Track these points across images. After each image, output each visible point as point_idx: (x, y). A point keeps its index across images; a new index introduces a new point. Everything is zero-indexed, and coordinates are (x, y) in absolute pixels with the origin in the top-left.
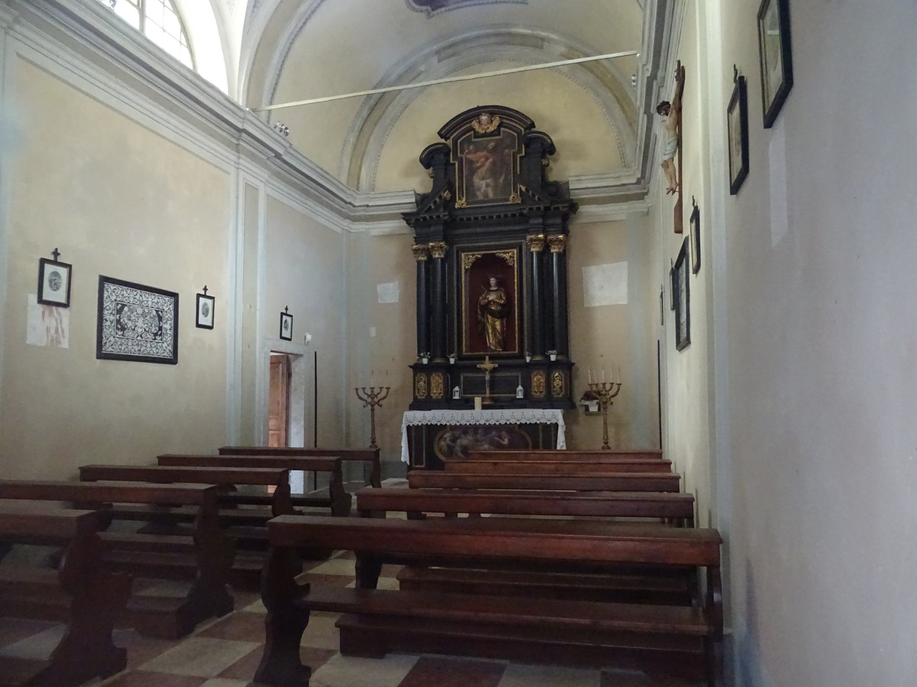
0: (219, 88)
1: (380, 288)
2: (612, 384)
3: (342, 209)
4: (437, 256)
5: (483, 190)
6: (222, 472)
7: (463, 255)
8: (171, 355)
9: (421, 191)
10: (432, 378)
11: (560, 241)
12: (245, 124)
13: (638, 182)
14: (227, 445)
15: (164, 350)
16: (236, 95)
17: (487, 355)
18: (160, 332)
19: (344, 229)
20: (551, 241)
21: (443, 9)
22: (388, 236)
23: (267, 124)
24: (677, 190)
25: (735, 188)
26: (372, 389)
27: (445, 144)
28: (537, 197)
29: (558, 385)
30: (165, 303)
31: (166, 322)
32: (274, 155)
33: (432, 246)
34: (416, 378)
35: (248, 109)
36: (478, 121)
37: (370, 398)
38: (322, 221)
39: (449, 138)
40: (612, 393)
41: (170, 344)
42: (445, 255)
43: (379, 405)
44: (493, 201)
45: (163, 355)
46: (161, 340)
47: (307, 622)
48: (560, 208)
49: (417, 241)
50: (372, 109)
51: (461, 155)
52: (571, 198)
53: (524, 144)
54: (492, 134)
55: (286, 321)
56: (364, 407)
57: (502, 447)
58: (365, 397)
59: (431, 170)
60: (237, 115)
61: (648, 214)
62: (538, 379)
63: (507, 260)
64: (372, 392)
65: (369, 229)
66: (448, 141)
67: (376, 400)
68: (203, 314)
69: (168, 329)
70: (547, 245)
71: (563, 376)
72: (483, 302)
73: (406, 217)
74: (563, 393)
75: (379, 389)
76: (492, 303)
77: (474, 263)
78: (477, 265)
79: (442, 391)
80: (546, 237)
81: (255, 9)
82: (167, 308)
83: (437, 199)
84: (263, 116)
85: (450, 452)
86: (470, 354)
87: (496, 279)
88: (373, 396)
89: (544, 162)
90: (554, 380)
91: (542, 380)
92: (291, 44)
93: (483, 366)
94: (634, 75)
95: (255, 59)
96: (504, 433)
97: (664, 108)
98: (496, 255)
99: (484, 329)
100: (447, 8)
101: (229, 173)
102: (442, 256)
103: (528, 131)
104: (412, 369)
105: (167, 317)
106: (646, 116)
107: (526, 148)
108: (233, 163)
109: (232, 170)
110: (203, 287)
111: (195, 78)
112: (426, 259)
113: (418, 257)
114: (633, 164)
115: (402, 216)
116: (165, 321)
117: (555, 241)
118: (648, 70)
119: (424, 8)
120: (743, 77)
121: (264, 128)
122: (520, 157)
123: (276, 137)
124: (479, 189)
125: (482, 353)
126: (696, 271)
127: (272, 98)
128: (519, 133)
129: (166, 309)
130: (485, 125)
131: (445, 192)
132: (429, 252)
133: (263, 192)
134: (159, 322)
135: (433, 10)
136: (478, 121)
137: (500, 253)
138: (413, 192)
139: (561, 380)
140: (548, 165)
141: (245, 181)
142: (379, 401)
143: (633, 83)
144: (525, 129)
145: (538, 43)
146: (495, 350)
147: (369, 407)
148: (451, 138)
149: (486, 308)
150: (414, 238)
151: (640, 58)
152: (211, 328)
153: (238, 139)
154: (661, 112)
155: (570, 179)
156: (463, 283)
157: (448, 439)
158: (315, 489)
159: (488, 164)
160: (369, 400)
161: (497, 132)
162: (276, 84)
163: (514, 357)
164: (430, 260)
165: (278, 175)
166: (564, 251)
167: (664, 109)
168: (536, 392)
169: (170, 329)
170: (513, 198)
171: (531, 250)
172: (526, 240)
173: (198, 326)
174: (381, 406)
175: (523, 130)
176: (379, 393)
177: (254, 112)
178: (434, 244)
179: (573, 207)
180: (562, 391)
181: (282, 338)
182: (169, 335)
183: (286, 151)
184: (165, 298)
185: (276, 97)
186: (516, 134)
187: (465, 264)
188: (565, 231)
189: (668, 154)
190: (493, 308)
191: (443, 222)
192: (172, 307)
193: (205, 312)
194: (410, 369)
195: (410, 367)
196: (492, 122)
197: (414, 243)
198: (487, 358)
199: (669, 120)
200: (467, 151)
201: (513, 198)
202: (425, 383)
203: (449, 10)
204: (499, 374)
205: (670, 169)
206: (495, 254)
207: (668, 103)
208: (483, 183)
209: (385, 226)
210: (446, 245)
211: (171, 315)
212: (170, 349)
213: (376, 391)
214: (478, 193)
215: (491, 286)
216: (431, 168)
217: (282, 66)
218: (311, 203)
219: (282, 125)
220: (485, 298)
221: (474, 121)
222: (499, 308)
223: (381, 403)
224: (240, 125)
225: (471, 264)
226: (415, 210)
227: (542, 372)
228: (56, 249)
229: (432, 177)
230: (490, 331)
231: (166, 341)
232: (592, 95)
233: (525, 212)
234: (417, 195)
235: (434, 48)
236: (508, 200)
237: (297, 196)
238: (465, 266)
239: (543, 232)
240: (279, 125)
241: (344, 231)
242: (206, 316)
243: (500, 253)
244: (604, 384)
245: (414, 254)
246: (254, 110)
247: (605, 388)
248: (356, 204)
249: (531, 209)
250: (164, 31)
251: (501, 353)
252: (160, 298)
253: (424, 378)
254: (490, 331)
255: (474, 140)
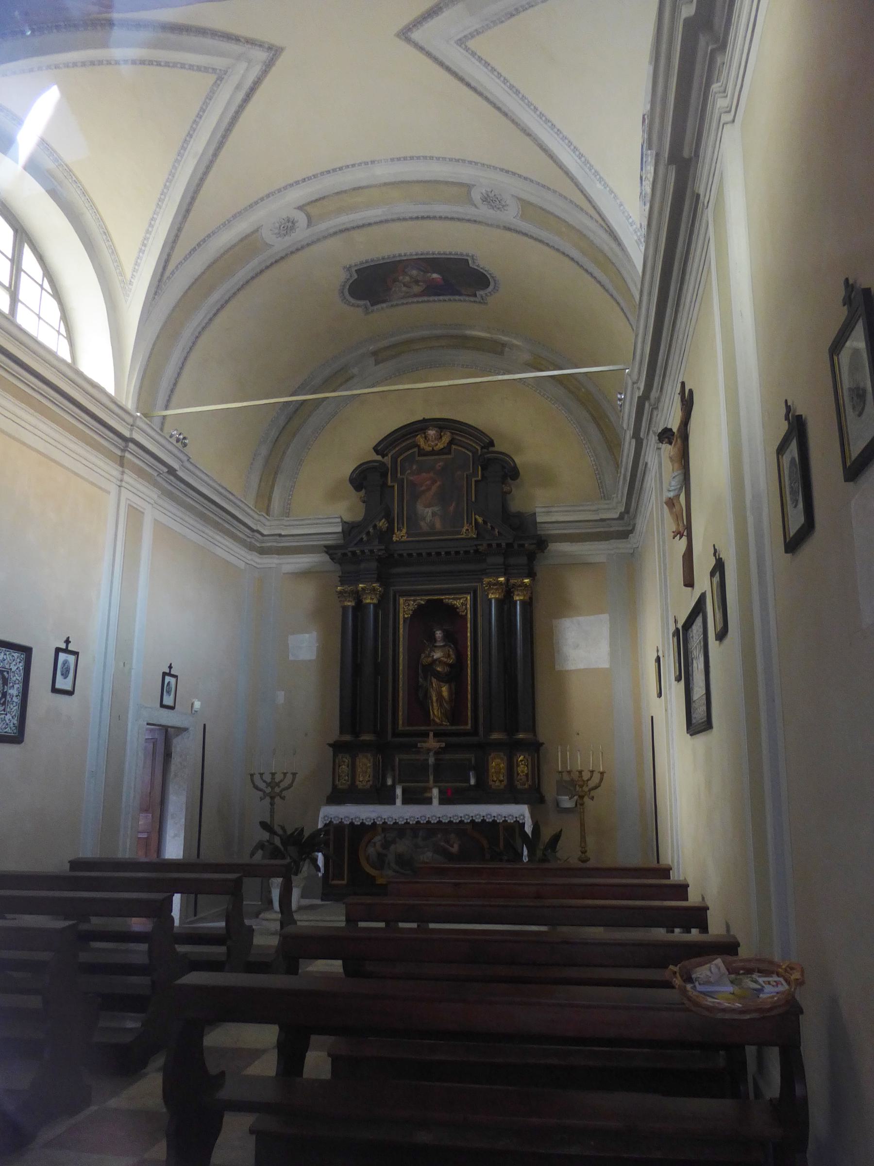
0: (99, 382)
1: (292, 640)
2: (592, 772)
3: (263, 545)
4: (368, 601)
5: (428, 519)
6: (86, 900)
7: (401, 601)
8: (15, 731)
9: (348, 518)
10: (358, 760)
11: (526, 586)
12: (134, 432)
13: (621, 517)
14: (81, 856)
15: (7, 724)
16: (125, 396)
17: (432, 731)
18: (4, 699)
19: (248, 564)
20: (514, 585)
21: (384, 305)
22: (305, 574)
23: (159, 431)
24: (685, 533)
25: (793, 545)
26: (273, 774)
27: (381, 461)
28: (497, 531)
29: (523, 772)
30: (14, 660)
31: (13, 686)
32: (166, 470)
33: (362, 588)
34: (337, 761)
35: (139, 414)
36: (423, 436)
37: (269, 787)
38: (219, 552)
39: (387, 455)
40: (592, 784)
41: (15, 715)
42: (379, 601)
43: (280, 797)
44: (441, 533)
45: (5, 731)
46: (4, 710)
47: (219, 1130)
48: (526, 545)
49: (343, 581)
50: (290, 419)
51: (401, 477)
52: (539, 533)
53: (481, 466)
54: (441, 452)
55: (169, 683)
56: (261, 799)
57: (450, 857)
58: (262, 785)
59: (362, 493)
60: (124, 421)
61: (632, 554)
62: (497, 764)
63: (457, 608)
64: (273, 778)
65: (280, 564)
66: (386, 458)
67: (277, 790)
68: (62, 675)
69: (15, 695)
70: (509, 592)
71: (530, 760)
72: (425, 661)
73: (329, 550)
74: (530, 782)
75: (282, 775)
76: (437, 662)
77: (415, 612)
78: (420, 612)
79: (371, 778)
80: (507, 580)
81: (156, 297)
82: (16, 667)
83: (371, 530)
84: (157, 422)
85: (380, 862)
86: (408, 728)
87: (443, 632)
88: (273, 784)
89: (506, 489)
90: (518, 766)
91: (502, 765)
92: (197, 337)
93: (424, 745)
94: (621, 394)
95: (151, 354)
96: (453, 836)
97: (666, 435)
98: (444, 601)
99: (427, 696)
100: (390, 304)
101: (109, 493)
102: (375, 601)
103: (486, 450)
104: (331, 749)
105: (14, 679)
106: (634, 442)
107: (483, 469)
108: (115, 480)
109: (113, 489)
110: (65, 639)
111: (73, 372)
112: (354, 604)
113: (344, 601)
114: (615, 495)
115: (325, 549)
116: (11, 684)
117: (520, 586)
118: (639, 389)
119: (361, 303)
120: (800, 416)
121: (157, 437)
122: (476, 481)
123: (170, 447)
124: (424, 519)
125: (423, 728)
126: (721, 636)
127: (169, 401)
128: (474, 453)
129: (14, 668)
130: (432, 441)
131: (380, 521)
132: (358, 597)
133: (150, 516)
134: (3, 686)
135: (372, 305)
136: (423, 436)
137: (449, 599)
138: (339, 520)
139: (527, 766)
140: (510, 492)
141: (128, 502)
142: (281, 791)
143: (619, 402)
144: (482, 448)
145: (497, 348)
146: (441, 725)
147: (268, 800)
148: (390, 456)
149: (429, 669)
150: (339, 577)
151: (629, 374)
152: (70, 693)
153: (123, 450)
154: (663, 441)
155: (538, 510)
156: (401, 636)
157: (378, 844)
158: (195, 916)
159: (434, 488)
160: (269, 790)
161: (446, 451)
162: (175, 384)
163: (465, 734)
164: (359, 607)
165: (170, 496)
166: (531, 598)
167: (666, 437)
168: (495, 781)
169: (17, 696)
170: (467, 531)
171: (490, 597)
172: (482, 584)
173: (55, 690)
174: (283, 798)
175: (479, 448)
176: (281, 781)
177: (146, 417)
178: (365, 585)
179: (542, 543)
180: (528, 780)
181: (162, 706)
182: (15, 704)
183: (182, 465)
184: (13, 654)
185: (174, 399)
186: (470, 454)
187: (404, 611)
188: (531, 574)
189: (675, 490)
190: (438, 669)
191: (377, 557)
192: (21, 666)
193: (64, 673)
194: (329, 748)
195: (330, 745)
196: (441, 437)
197: (339, 583)
198: (431, 734)
199: (668, 450)
200: (409, 471)
201: (467, 531)
202: (348, 767)
203: (392, 306)
204: (448, 756)
205: (677, 507)
206: (442, 599)
207: (671, 430)
208: (428, 512)
209: (298, 560)
210: (380, 586)
211: (20, 677)
212: (15, 722)
213: (278, 778)
214: (422, 524)
215: (435, 641)
216: (363, 491)
217: (183, 364)
218: (210, 531)
219: (180, 434)
220: (429, 656)
221: (419, 436)
222: (447, 669)
223: (284, 793)
224: (127, 434)
225: (411, 612)
226: (341, 542)
227: (502, 754)
228: (68, 638)
229: (364, 502)
230: (434, 699)
231: (10, 712)
232: (563, 411)
233: (481, 548)
234: (344, 523)
235: (371, 348)
236: (459, 533)
237: (192, 522)
238: (404, 615)
239: (504, 575)
240: (177, 434)
241: (248, 566)
242: (65, 678)
243: (448, 599)
244: (580, 772)
245: (339, 597)
246: (145, 415)
247: (582, 777)
248: (265, 533)
249: (490, 545)
250: (40, 318)
251: (450, 728)
252: (8, 653)
253: (347, 759)
254: (434, 699)
255: (417, 458)
